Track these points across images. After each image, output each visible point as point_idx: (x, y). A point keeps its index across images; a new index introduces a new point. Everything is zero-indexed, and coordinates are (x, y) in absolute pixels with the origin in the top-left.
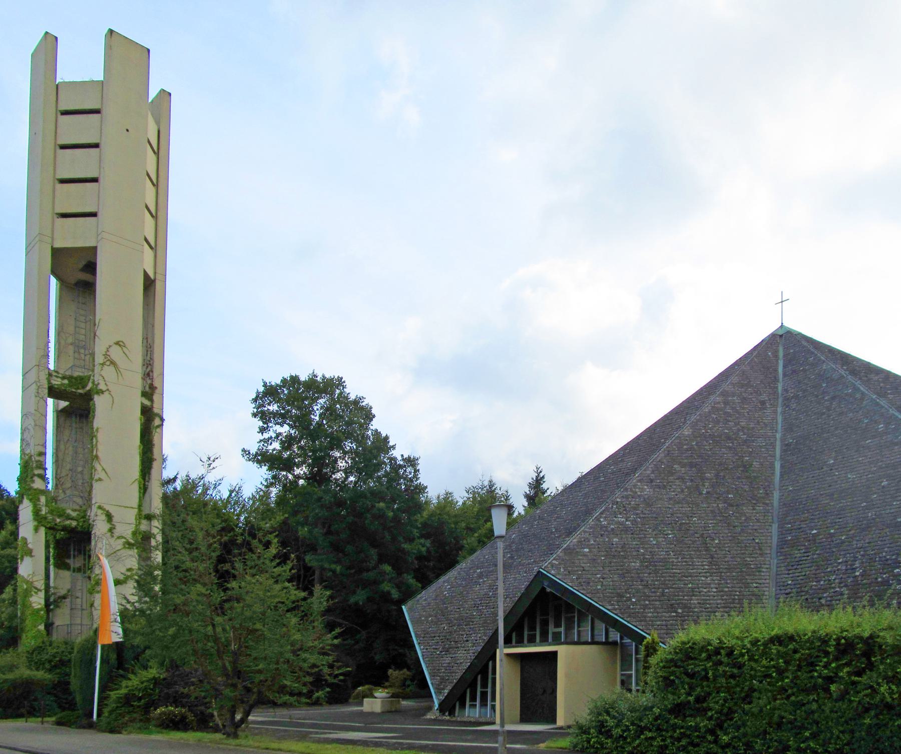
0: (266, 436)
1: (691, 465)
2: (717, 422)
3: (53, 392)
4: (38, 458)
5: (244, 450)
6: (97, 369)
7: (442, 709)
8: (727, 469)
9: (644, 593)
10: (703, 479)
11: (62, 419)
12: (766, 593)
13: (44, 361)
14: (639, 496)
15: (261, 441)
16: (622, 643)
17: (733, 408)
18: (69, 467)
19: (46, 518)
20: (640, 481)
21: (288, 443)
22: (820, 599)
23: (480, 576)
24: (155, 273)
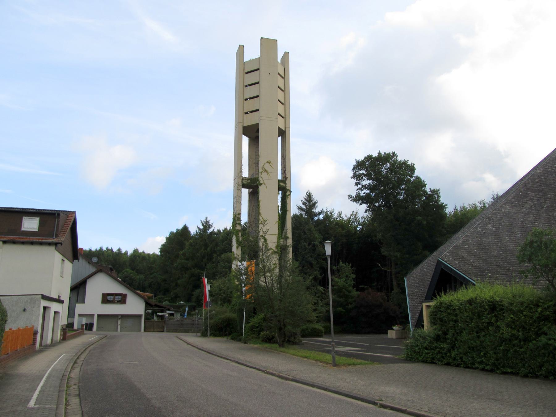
0: (360, 186)
3: (244, 186)
5: (349, 196)
6: (260, 174)
9: (497, 270)
14: (503, 213)
20: (505, 204)
21: (371, 188)
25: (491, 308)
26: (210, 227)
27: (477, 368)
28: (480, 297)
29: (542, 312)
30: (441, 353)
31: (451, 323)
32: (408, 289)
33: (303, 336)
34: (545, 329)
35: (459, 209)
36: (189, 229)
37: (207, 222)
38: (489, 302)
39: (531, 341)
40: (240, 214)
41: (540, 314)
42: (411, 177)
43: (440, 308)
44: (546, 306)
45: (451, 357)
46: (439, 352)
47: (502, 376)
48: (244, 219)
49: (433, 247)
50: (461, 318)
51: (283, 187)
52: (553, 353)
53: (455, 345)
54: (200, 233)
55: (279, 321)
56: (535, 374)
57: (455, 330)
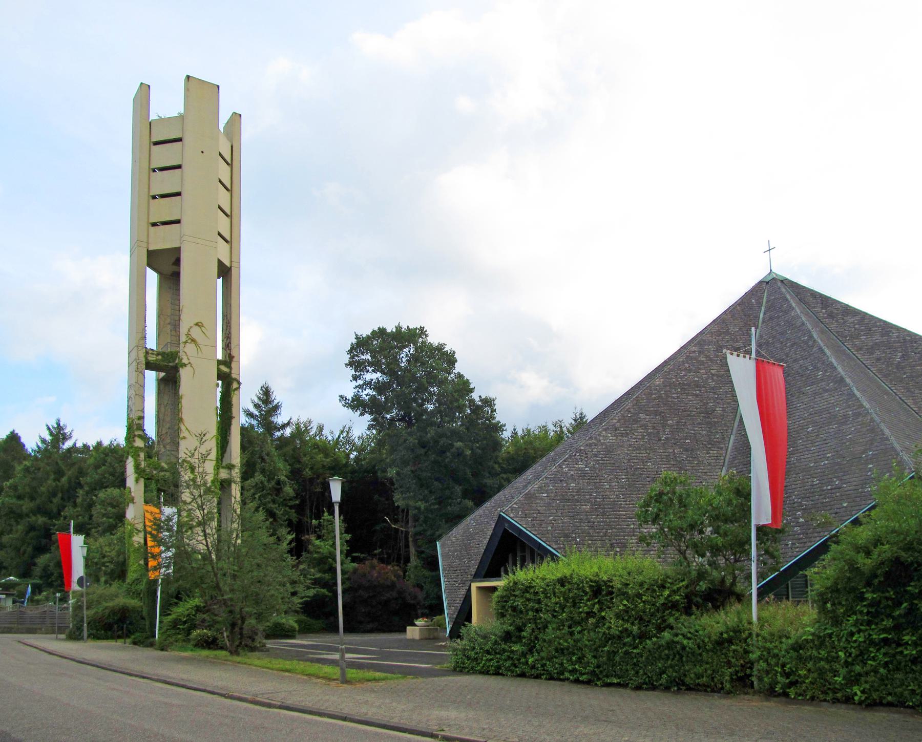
0: (360, 382)
1: (656, 413)
2: (689, 370)
3: (149, 366)
4: (137, 422)
6: (182, 345)
8: (689, 415)
10: (664, 426)
11: (162, 386)
13: (142, 342)
14: (602, 444)
15: (356, 387)
17: (707, 357)
18: (168, 425)
19: (144, 471)
20: (605, 430)
21: (380, 387)
24: (231, 262)
25: (593, 591)
26: (65, 438)
27: (568, 679)
28: (577, 575)
29: (669, 596)
30: (512, 658)
31: (530, 613)
32: (443, 560)
33: (268, 637)
34: (671, 620)
35: (520, 433)
36: (22, 440)
37: (59, 428)
38: (591, 581)
39: (650, 638)
40: (143, 418)
41: (666, 599)
42: (450, 373)
43: (514, 591)
44: (675, 588)
45: (527, 662)
46: (509, 658)
47: (604, 689)
48: (151, 428)
49: (480, 496)
50: (546, 605)
51: (225, 373)
52: (679, 654)
53: (534, 647)
54: (46, 450)
55: (231, 612)
56: (652, 684)
57: (536, 623)
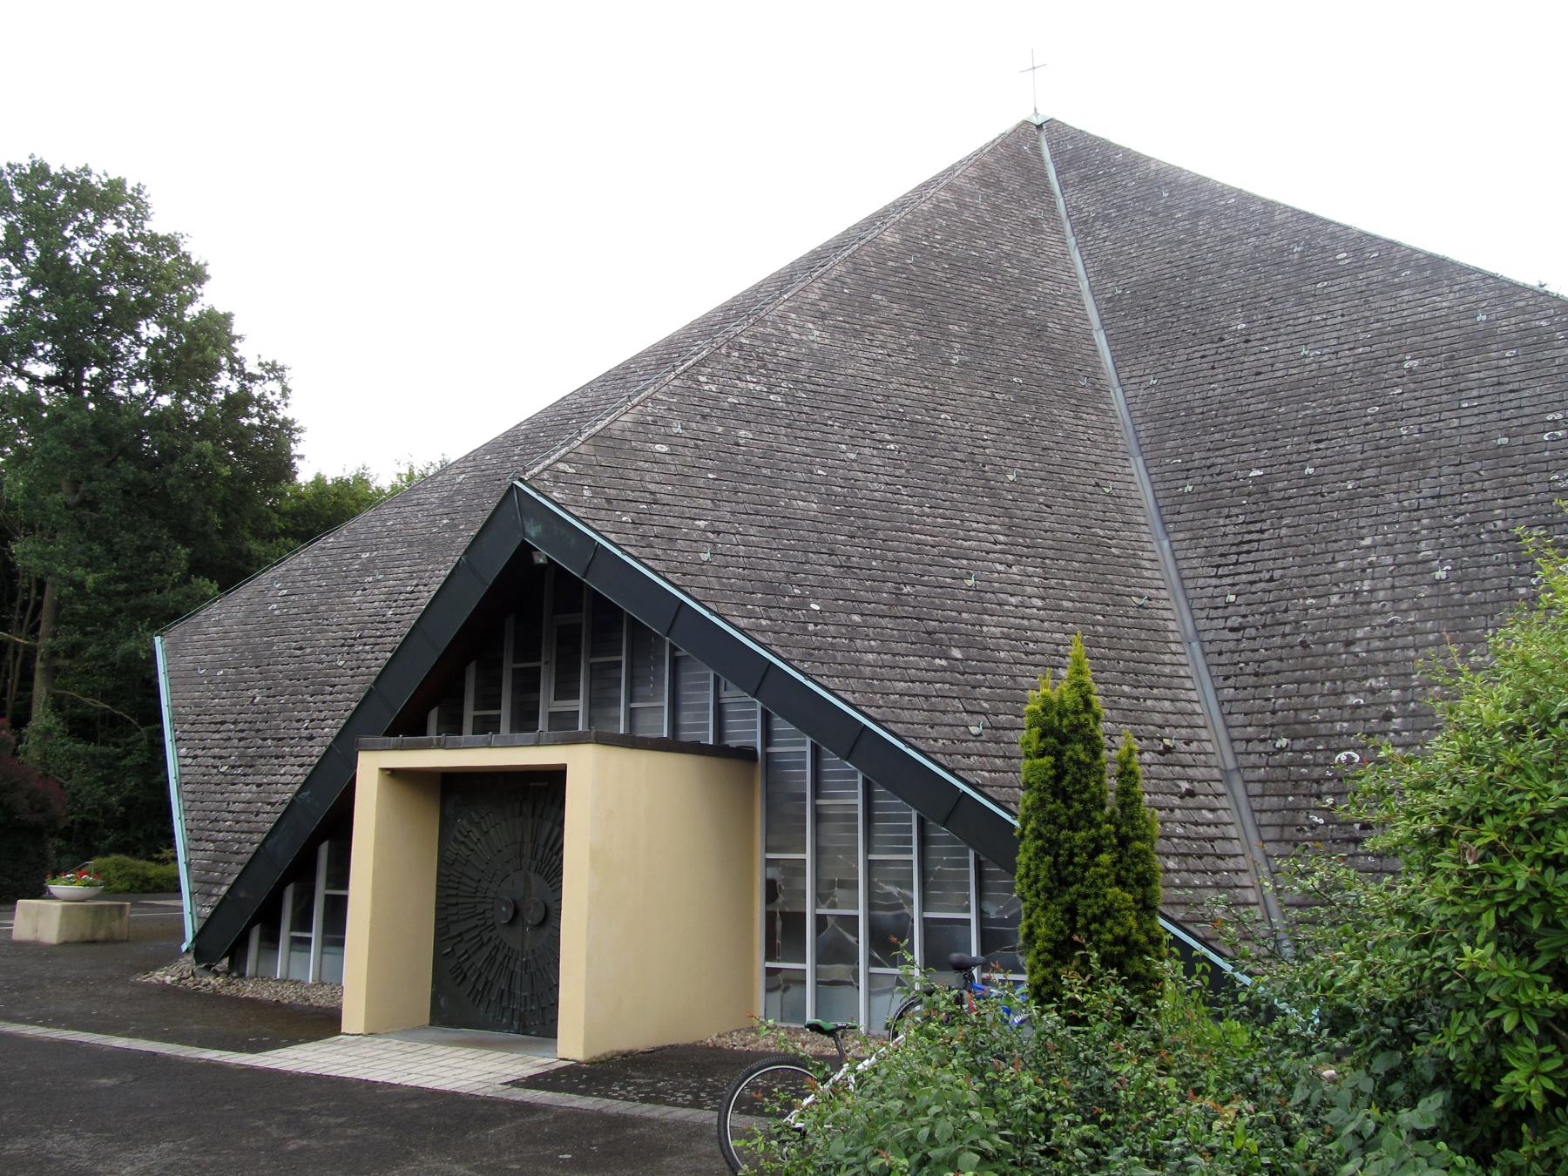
7: (203, 952)
12: (1172, 626)
16: (767, 755)
22: (1349, 643)
23: (366, 569)
